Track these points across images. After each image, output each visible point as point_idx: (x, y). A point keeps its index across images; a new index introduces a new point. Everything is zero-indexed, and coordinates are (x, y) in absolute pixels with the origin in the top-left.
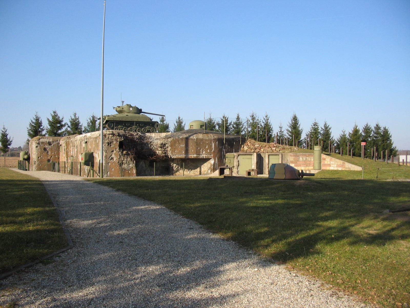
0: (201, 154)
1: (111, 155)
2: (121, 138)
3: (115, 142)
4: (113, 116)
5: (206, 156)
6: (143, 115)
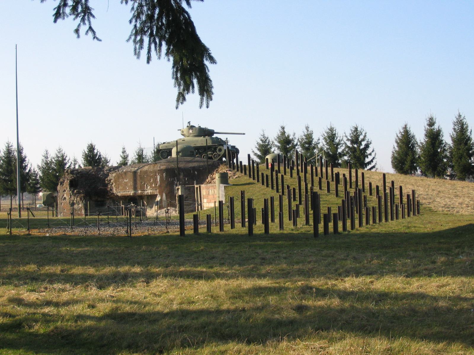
0: (145, 189)
1: (63, 195)
5: (151, 191)
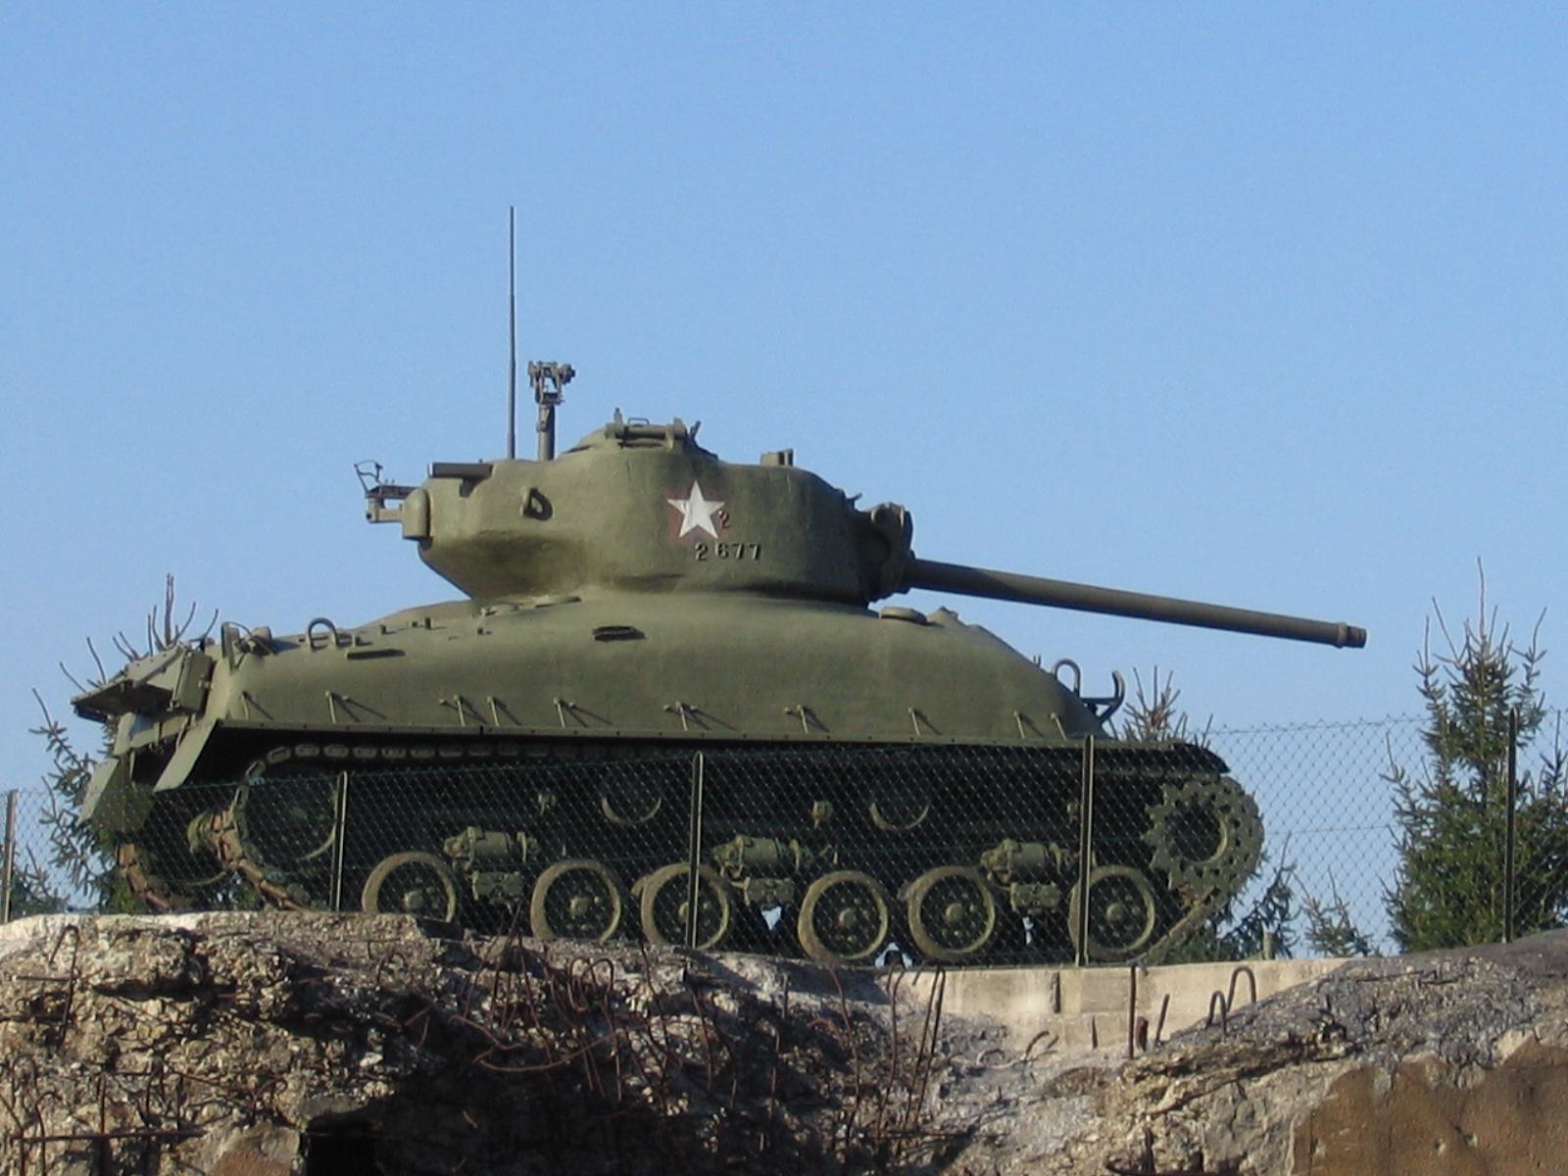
2: (348, 1060)
3: (220, 1143)
4: (342, 639)
6: (917, 619)
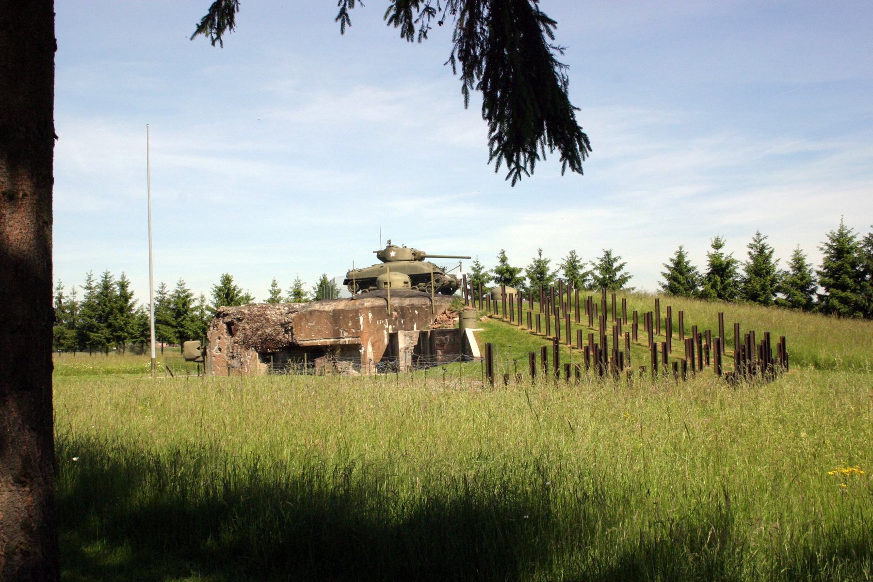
0: (341, 336)
5: (351, 339)
